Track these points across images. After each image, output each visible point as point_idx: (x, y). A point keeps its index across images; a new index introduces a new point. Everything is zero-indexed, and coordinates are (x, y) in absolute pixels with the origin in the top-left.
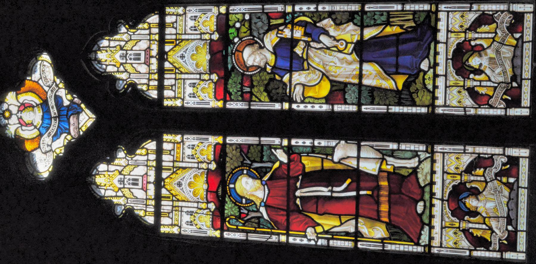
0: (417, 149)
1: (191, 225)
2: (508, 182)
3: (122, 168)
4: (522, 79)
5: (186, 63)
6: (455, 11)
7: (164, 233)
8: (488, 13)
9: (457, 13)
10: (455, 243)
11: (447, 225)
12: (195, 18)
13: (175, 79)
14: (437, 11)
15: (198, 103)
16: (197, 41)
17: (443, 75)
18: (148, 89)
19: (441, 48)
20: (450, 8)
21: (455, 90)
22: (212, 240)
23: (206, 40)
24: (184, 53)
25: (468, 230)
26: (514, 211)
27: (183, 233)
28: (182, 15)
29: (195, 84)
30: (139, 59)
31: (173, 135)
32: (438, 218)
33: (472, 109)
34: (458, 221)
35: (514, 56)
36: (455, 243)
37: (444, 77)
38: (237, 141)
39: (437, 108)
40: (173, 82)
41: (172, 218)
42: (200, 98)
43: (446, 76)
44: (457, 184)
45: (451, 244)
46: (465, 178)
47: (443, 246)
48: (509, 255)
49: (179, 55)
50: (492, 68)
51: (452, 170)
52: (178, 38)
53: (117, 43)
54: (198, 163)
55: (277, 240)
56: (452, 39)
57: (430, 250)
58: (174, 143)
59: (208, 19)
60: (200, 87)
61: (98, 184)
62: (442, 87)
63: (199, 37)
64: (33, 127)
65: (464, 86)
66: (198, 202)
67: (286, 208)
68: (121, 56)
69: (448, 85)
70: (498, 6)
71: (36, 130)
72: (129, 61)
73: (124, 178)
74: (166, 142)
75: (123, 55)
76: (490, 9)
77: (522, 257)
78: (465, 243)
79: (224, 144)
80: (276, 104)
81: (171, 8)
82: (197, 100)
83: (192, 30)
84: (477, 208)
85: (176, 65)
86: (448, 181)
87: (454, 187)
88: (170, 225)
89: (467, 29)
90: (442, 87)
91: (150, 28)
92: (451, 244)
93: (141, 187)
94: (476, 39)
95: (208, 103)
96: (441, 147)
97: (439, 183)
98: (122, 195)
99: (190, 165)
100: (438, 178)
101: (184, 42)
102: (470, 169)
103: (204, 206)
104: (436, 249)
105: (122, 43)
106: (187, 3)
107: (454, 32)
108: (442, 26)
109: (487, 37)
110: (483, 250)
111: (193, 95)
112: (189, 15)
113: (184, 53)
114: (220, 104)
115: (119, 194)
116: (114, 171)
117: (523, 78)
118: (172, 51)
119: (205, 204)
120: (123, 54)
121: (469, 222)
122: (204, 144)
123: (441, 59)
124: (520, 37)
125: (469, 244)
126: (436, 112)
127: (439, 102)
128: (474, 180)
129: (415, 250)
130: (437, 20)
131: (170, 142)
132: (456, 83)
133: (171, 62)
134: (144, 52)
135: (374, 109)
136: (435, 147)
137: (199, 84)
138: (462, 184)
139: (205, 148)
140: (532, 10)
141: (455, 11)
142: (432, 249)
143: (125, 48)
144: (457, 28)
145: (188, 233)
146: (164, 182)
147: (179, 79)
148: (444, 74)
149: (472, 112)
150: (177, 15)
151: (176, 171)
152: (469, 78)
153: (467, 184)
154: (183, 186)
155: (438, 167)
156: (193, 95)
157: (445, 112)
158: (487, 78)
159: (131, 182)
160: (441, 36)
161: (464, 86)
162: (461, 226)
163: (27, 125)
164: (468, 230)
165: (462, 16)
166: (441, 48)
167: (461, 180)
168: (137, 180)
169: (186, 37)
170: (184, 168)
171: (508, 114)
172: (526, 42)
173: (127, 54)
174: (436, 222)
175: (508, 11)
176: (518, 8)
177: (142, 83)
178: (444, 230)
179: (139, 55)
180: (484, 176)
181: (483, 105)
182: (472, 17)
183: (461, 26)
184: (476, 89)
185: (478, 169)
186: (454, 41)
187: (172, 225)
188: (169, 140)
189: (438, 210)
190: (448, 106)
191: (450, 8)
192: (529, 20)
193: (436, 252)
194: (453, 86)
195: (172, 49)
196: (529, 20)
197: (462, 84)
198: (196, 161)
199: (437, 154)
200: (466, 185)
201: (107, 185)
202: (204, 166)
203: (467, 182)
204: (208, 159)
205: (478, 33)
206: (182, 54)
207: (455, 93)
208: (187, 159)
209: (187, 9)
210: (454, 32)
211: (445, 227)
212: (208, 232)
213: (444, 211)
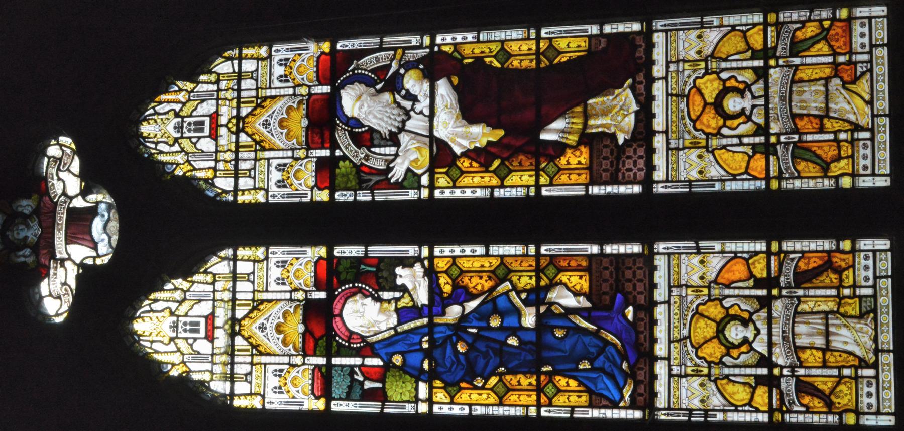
1: (280, 393)
3: (180, 106)
5: (272, 135)
7: (239, 408)
12: (283, 264)
13: (252, 364)
14: (652, 254)
15: (287, 403)
16: (283, 303)
17: (663, 132)
18: (212, 380)
20: (668, 25)
22: (312, 414)
23: (299, 301)
24: (265, 322)
27: (268, 406)
28: (263, 260)
29: (285, 165)
30: (202, 130)
31: (253, 248)
38: (353, 45)
40: (247, 368)
41: (254, 178)
42: (290, 394)
49: (261, 121)
52: (254, 362)
53: (165, 305)
54: (294, 88)
55: (413, 412)
58: (254, 261)
59: (302, 267)
60: (289, 378)
61: (145, 134)
62: (661, 98)
63: (291, 91)
66: (290, 356)
67: (426, 133)
68: (175, 128)
72: (187, 134)
73: (183, 121)
74: (242, 260)
75: (179, 130)
77: (888, 421)
79: (329, 365)
80: (410, 191)
81: (247, 249)
82: (285, 397)
83: (281, 81)
85: (257, 137)
88: (248, 395)
90: (661, 98)
91: (218, 82)
93: (208, 134)
95: (301, 404)
96: (663, 23)
97: (663, 268)
98: (179, 149)
99: (282, 92)
101: (268, 100)
103: (298, 360)
104: (661, 185)
105: (177, 107)
108: (661, 314)
111: (279, 390)
112: (276, 58)
113: (265, 322)
114: (320, 405)
115: (176, 148)
116: (163, 311)
118: (247, 319)
119: (300, 357)
120: (178, 122)
122: (300, 261)
127: (661, 402)
130: (651, 46)
131: (252, 58)
133: (250, 133)
134: (208, 118)
137: (292, 264)
139: (302, 267)
141: (689, 29)
142: (655, 186)
143: (177, 313)
145: (276, 406)
146: (240, 325)
147: (261, 159)
148: (664, 75)
150: (258, 59)
151: (258, 306)
154: (268, 330)
155: (660, 277)
156: (279, 390)
159: (188, 327)
168: (198, 324)
169: (269, 296)
170: (273, 97)
173: (183, 121)
177: (199, 372)
179: (198, 324)
183: (702, 278)
187: (251, 394)
188: (246, 258)
190: (672, 182)
191: (668, 25)
195: (250, 114)
198: (288, 288)
199: (658, 257)
201: (158, 136)
202: (300, 295)
204: (306, 285)
206: (263, 324)
208: (276, 84)
209: (274, 49)
212: (306, 402)
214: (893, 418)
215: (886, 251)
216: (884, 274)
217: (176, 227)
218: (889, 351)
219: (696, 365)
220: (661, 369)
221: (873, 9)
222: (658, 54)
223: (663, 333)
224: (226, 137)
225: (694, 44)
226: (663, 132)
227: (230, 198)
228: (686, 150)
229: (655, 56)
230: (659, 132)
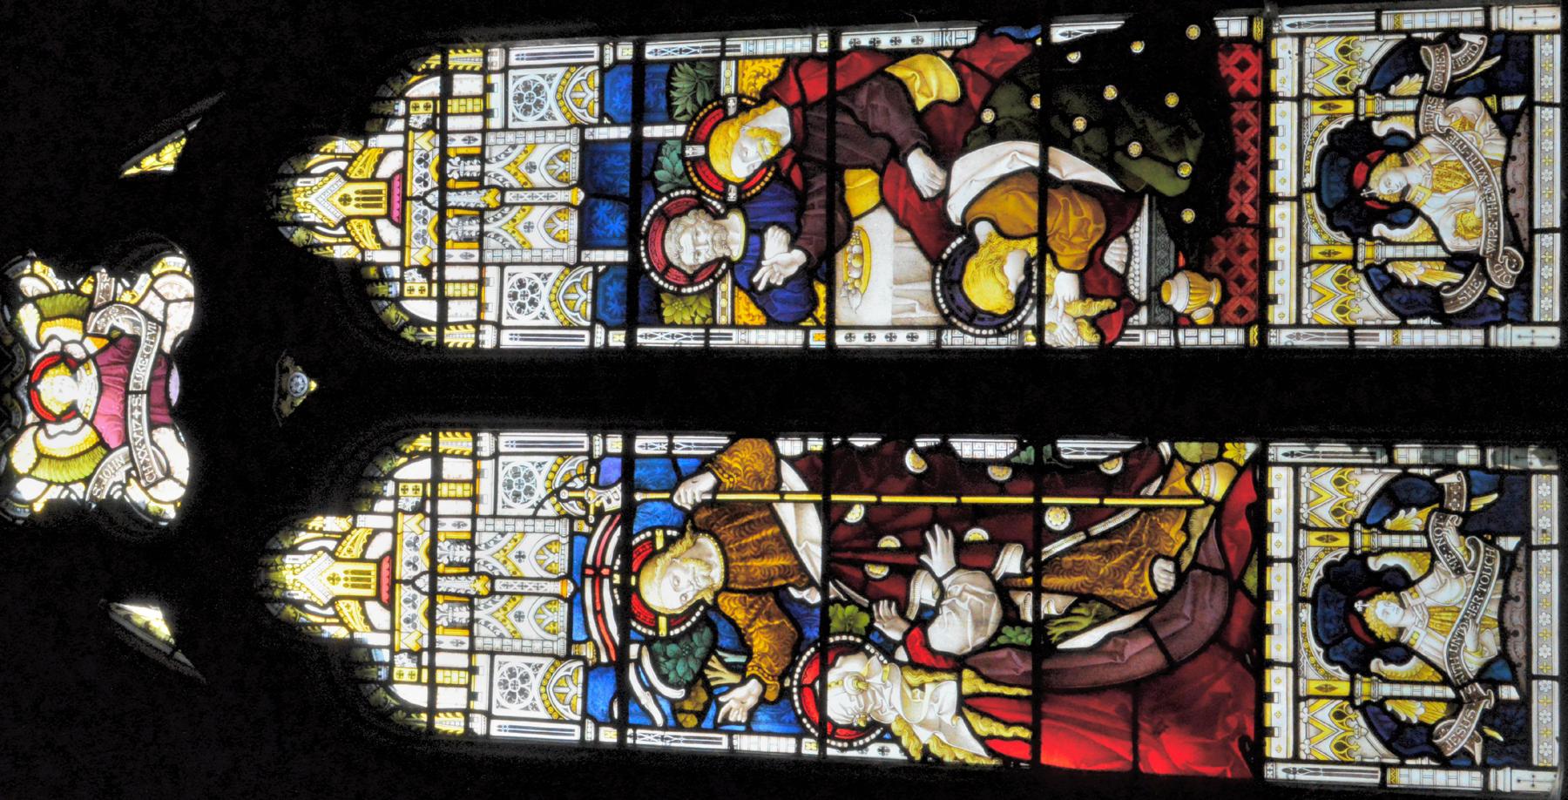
0: (1217, 332)
2: (1501, 112)
4: (1530, 677)
6: (1318, 465)
8: (1425, 35)
9: (1322, 469)
10: (1340, 747)
11: (1316, 254)
17: (1286, 560)
19: (1278, 681)
21: (1324, 711)
25: (1383, 267)
26: (1522, 191)
32: (1284, 598)
33: (1382, 333)
34: (1345, 675)
35: (1509, 157)
36: (1340, 747)
37: (1290, 671)
39: (1273, 332)
43: (1295, 665)
44: (1342, 126)
45: (1326, 750)
46: (1363, 540)
47: (1303, 756)
48: (1507, 779)
50: (1444, 192)
51: (1324, 515)
56: (1316, 121)
57: (1263, 337)
64: (77, 422)
65: (1353, 262)
69: (1305, 260)
70: (1455, 16)
71: (87, 428)
76: (1431, 25)
77: (1547, 782)
78: (1369, 747)
84: (1401, 631)
86: (1311, 553)
87: (1328, 567)
89: (1354, 522)
92: (1326, 750)
94: (1386, 116)
96: (1288, 450)
100: (1283, 147)
102: (1381, 81)
104: (1281, 766)
106: (512, 38)
107: (1317, 529)
108: (1278, 715)
109: (1418, 694)
110: (1431, 327)
117: (1537, 226)
121: (1387, 242)
123: (1279, 611)
124: (1523, 106)
125: (1383, 750)
126: (1272, 342)
127: (1278, 746)
128: (1391, 116)
129: (1217, 342)
132: (1329, 253)
135: (1080, 451)
136: (1271, 450)
138: (1357, 559)
140: (1556, 23)
141: (1318, 465)
144: (1327, 84)
148: (1290, 554)
149: (1384, 339)
152: (1369, 237)
153: (1375, 124)
157: (1300, 777)
158: (1429, 236)
160: (1279, 543)
161: (1353, 262)
162: (1360, 256)
163: (60, 419)
164: (1383, 267)
165: (1344, 51)
166: (1283, 216)
167: (1356, 113)
171: (1492, 787)
172: (1539, 548)
174: (1281, 282)
175: (1485, 30)
176: (1511, 19)
178: (1302, 704)
180: (1425, 533)
181: (1415, 757)
182: (1373, 50)
184: (1390, 706)
185: (1402, 512)
186: (1319, 556)
189: (1287, 177)
192: (1548, 53)
193: (1282, 776)
194: (1318, 697)
196: (1548, 53)
197: (1347, 253)
200: (1370, 129)
203: (1373, 118)
205: (1394, 98)
207: (1328, 720)
210: (1317, 529)
211: (1309, 264)
213: (1303, 645)
214: (1556, 332)
215: (1552, 32)
216: (1547, 225)
217: (315, 386)
218: (1552, 230)
219: (1327, 676)
220: (1278, 682)
221: (1526, 343)
222: (1278, 612)
223: (1287, 285)
224: (421, 220)
225: (1327, 731)
226: (1286, 560)
227: (431, 335)
228: (1311, 701)
229: (1272, 516)
230: (1280, 560)
